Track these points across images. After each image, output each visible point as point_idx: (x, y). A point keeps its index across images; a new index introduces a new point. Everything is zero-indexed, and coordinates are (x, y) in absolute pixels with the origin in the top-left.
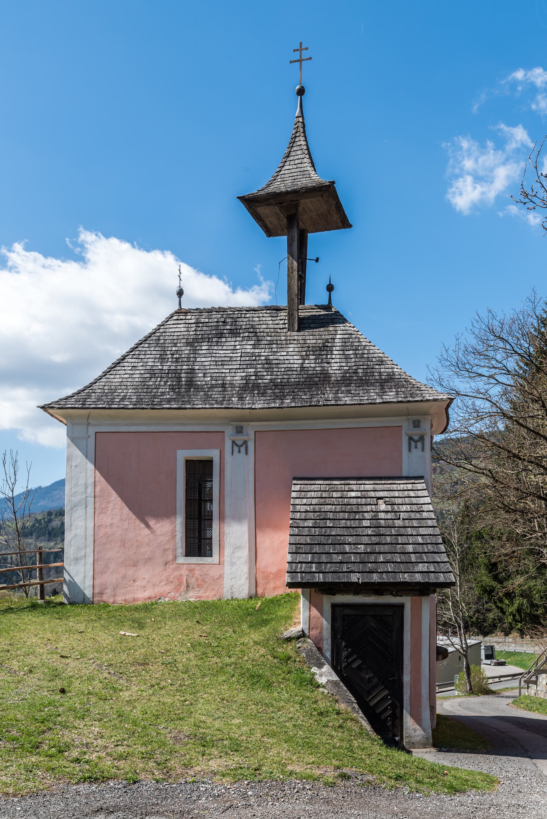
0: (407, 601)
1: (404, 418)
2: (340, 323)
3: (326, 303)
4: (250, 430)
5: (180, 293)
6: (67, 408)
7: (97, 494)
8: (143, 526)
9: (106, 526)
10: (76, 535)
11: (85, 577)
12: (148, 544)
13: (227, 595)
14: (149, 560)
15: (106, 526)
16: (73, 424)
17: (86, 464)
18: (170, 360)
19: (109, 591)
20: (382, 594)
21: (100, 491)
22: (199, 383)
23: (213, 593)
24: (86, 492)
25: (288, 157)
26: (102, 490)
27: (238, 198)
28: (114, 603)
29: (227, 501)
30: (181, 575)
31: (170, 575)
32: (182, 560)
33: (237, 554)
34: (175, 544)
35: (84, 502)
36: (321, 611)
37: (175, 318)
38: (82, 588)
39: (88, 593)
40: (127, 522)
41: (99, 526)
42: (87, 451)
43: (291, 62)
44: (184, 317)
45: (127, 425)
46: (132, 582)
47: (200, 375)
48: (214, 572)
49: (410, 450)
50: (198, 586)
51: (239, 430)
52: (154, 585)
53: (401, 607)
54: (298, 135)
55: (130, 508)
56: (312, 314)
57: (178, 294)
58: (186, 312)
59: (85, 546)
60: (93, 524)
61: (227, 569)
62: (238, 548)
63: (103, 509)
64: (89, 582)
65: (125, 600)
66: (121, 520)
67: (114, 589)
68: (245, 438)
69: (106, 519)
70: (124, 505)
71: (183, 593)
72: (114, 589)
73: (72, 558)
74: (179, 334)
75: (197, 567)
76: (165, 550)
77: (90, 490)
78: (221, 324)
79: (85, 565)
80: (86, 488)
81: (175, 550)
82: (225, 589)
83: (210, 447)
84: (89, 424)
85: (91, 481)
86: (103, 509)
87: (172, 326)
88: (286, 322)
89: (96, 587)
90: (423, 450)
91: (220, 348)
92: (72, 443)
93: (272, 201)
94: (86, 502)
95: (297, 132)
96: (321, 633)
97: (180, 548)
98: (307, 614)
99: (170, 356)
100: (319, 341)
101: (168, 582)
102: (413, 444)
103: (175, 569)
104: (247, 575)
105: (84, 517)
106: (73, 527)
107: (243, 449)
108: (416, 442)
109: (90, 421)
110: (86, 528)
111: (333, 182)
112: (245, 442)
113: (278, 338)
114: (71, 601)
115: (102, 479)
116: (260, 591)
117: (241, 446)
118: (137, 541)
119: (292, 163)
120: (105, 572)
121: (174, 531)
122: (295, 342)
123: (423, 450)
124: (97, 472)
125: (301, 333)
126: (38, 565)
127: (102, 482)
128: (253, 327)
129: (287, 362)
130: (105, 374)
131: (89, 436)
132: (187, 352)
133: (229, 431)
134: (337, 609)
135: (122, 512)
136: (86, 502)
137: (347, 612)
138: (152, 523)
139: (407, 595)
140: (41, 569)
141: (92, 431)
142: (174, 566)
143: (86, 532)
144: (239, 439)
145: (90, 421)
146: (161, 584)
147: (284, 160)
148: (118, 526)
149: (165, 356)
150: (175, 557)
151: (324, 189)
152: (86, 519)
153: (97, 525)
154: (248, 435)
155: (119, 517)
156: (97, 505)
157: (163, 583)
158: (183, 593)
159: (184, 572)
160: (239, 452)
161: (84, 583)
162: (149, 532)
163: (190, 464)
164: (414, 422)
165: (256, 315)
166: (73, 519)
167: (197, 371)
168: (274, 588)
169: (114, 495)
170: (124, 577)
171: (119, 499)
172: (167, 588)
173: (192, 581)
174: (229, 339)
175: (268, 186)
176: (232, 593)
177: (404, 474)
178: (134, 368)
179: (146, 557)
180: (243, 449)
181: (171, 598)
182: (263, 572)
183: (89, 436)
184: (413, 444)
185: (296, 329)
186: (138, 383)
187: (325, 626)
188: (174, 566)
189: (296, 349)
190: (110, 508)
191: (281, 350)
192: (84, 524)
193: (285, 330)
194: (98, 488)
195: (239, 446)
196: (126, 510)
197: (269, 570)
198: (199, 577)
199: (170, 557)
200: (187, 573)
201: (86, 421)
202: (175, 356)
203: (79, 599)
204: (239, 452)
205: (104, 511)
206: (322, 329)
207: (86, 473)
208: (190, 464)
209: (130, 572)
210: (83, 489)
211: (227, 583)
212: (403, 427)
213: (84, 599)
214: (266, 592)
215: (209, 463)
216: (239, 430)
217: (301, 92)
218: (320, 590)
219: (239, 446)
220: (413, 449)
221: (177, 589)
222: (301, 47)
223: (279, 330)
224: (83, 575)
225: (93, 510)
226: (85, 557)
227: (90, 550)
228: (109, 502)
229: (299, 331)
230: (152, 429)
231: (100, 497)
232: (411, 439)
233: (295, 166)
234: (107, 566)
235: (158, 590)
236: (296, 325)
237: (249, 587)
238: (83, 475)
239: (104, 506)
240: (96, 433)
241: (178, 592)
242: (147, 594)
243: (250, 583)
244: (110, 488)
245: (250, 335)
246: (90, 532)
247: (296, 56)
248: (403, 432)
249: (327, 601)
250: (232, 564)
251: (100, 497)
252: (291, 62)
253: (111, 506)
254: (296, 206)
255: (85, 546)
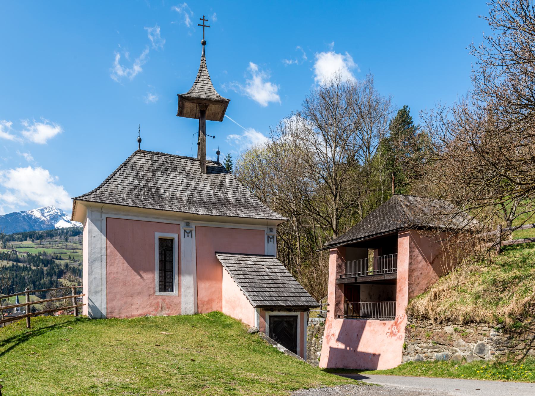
0: (298, 314)
1: (266, 226)
2: (226, 173)
3: (216, 160)
4: (193, 225)
5: (140, 141)
6: (91, 201)
7: (108, 254)
8: (136, 274)
9: (114, 273)
10: (95, 278)
11: (102, 303)
12: (139, 285)
13: (183, 313)
14: (139, 293)
15: (114, 273)
16: (92, 211)
17: (101, 236)
18: (142, 180)
19: (116, 311)
20: (272, 311)
21: (110, 252)
22: (163, 196)
23: (176, 312)
24: (101, 253)
25: (199, 78)
26: (111, 252)
27: (178, 95)
28: (120, 317)
29: (183, 263)
30: (158, 302)
31: (152, 302)
32: (158, 293)
33: (188, 291)
34: (155, 284)
35: (100, 258)
36: (265, 319)
37: (138, 154)
38: (100, 309)
39: (104, 312)
40: (127, 271)
41: (109, 273)
42: (101, 228)
43: (199, 25)
44: (143, 155)
45: (125, 215)
46: (130, 306)
47: (162, 191)
48: (176, 301)
49: (268, 242)
50: (168, 308)
51: (188, 225)
52: (143, 308)
53: (297, 317)
54: (203, 67)
55: (129, 263)
56: (210, 165)
57: (138, 141)
58: (144, 152)
59: (101, 284)
60: (106, 271)
61: (183, 299)
62: (189, 287)
63: (112, 263)
64: (104, 306)
65: (126, 316)
66: (123, 270)
67: (120, 310)
68: (191, 229)
69: (114, 269)
70: (125, 261)
71: (159, 312)
72: (120, 310)
73: (93, 291)
74: (143, 165)
75: (167, 298)
76: (149, 288)
77: (104, 251)
78: (165, 163)
79: (101, 296)
80: (101, 250)
81: (154, 288)
82: (182, 310)
83: (173, 232)
84: (102, 212)
85: (104, 246)
86: (112, 263)
87: (137, 159)
88: (199, 167)
89: (108, 309)
90: (274, 243)
91: (169, 177)
92: (91, 222)
93: (195, 101)
94: (101, 259)
95: (203, 65)
96: (265, 329)
97: (157, 288)
98: (259, 321)
99: (142, 177)
100: (219, 181)
101: (151, 306)
102: (270, 239)
103: (155, 299)
104: (193, 302)
105: (100, 267)
106: (93, 273)
107: (190, 235)
108: (271, 238)
109: (103, 210)
110: (102, 273)
111: (230, 100)
112: (191, 231)
113: (197, 176)
114: (94, 317)
115: (111, 245)
116: (200, 311)
117: (189, 233)
118: (133, 282)
119: (202, 82)
120: (114, 300)
121: (154, 278)
122: (207, 180)
123: (274, 243)
124: (108, 241)
125: (208, 175)
126: (73, 295)
127: (111, 247)
128: (183, 167)
129: (206, 190)
130: (106, 182)
131: (102, 220)
132: (151, 176)
133: (182, 224)
134: (272, 318)
135: (123, 266)
136: (101, 259)
137: (276, 319)
138: (141, 273)
139: (299, 311)
140: (75, 298)
141: (104, 216)
142: (154, 297)
143: (101, 276)
144: (188, 229)
145: (103, 210)
146: (147, 307)
147: (198, 79)
148: (121, 274)
149: (139, 177)
150: (155, 292)
151: (224, 102)
152: (101, 268)
153: (108, 273)
154: (192, 228)
155: (122, 268)
156: (108, 261)
157: (148, 306)
158: (159, 312)
159: (160, 300)
160: (188, 236)
161: (101, 306)
162: (140, 277)
163: (162, 241)
164: (270, 229)
165: (183, 161)
166: (93, 268)
167: (160, 189)
168: (207, 309)
169: (119, 255)
170: (125, 303)
171: (122, 258)
172: (151, 309)
173: (164, 305)
174: (172, 173)
175: (191, 92)
176: (186, 311)
177: (266, 254)
178: (122, 182)
179: (138, 291)
180: (190, 235)
181: (153, 315)
182: (201, 301)
183: (102, 220)
184: (270, 239)
185: (206, 172)
186: (128, 191)
187: (266, 326)
188: (154, 297)
189: (209, 184)
190: (116, 263)
191: (201, 183)
192: (100, 271)
193: (199, 172)
194: (109, 251)
195: (188, 233)
196: (126, 264)
197: (204, 300)
198: (168, 303)
199: (152, 292)
200: (161, 301)
201: (100, 210)
202: (145, 178)
203: (98, 316)
204: (188, 236)
205: (113, 264)
206: (218, 175)
207: (101, 241)
208: (162, 241)
209: (129, 300)
210: (99, 251)
211: (183, 306)
212: (181, 225)
213: (101, 316)
214: (203, 311)
215: (172, 240)
216: (188, 225)
217: (204, 43)
218: (264, 309)
219: (188, 233)
220: (270, 242)
221: (156, 310)
222: (202, 19)
223: (196, 172)
224: (100, 302)
225: (106, 263)
226: (101, 291)
227: (104, 287)
228: (115, 259)
229: (207, 173)
230: (140, 219)
231: (110, 255)
232: (268, 237)
233: (204, 85)
234: (115, 297)
235: (145, 311)
236: (206, 170)
237: (195, 309)
238: (99, 242)
239: (112, 261)
240: (107, 218)
241: (156, 311)
242: (139, 312)
243: (195, 306)
244: (116, 251)
245: (183, 172)
246: (104, 276)
247: (201, 22)
248: (265, 233)
249: (268, 314)
250: (186, 296)
251: (110, 255)
252: (199, 25)
253: (117, 262)
254: (207, 107)
255: (101, 284)
